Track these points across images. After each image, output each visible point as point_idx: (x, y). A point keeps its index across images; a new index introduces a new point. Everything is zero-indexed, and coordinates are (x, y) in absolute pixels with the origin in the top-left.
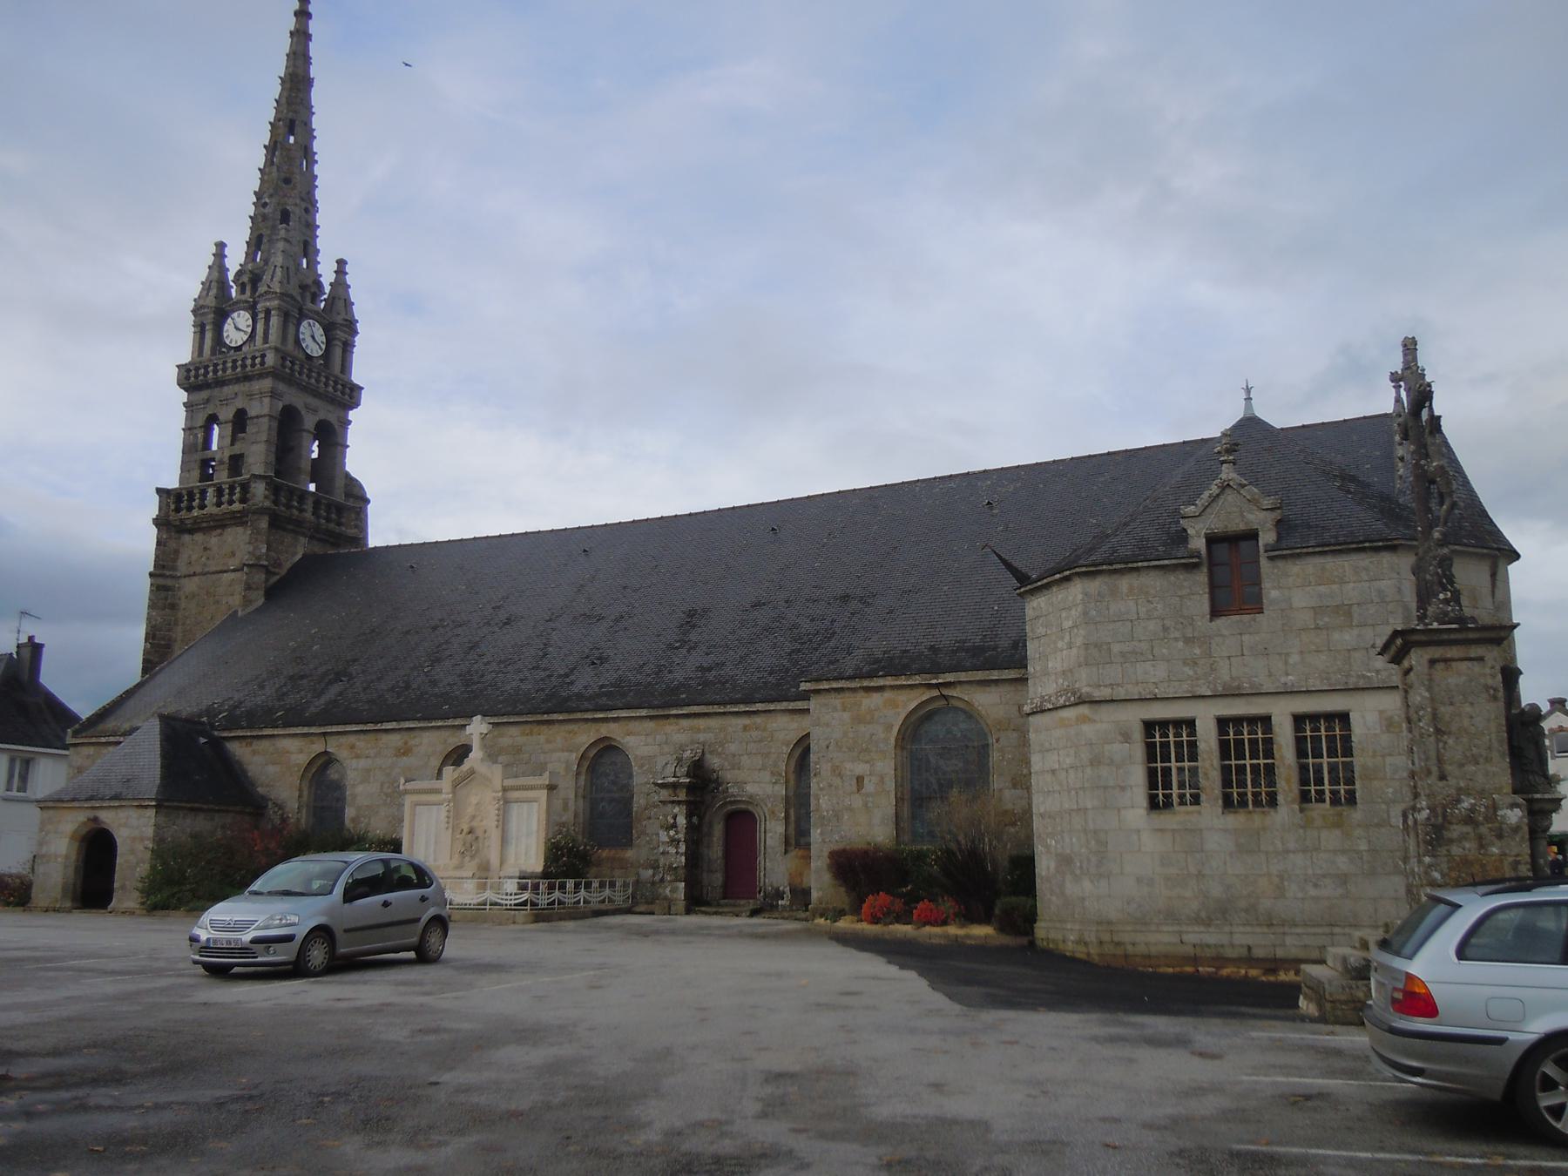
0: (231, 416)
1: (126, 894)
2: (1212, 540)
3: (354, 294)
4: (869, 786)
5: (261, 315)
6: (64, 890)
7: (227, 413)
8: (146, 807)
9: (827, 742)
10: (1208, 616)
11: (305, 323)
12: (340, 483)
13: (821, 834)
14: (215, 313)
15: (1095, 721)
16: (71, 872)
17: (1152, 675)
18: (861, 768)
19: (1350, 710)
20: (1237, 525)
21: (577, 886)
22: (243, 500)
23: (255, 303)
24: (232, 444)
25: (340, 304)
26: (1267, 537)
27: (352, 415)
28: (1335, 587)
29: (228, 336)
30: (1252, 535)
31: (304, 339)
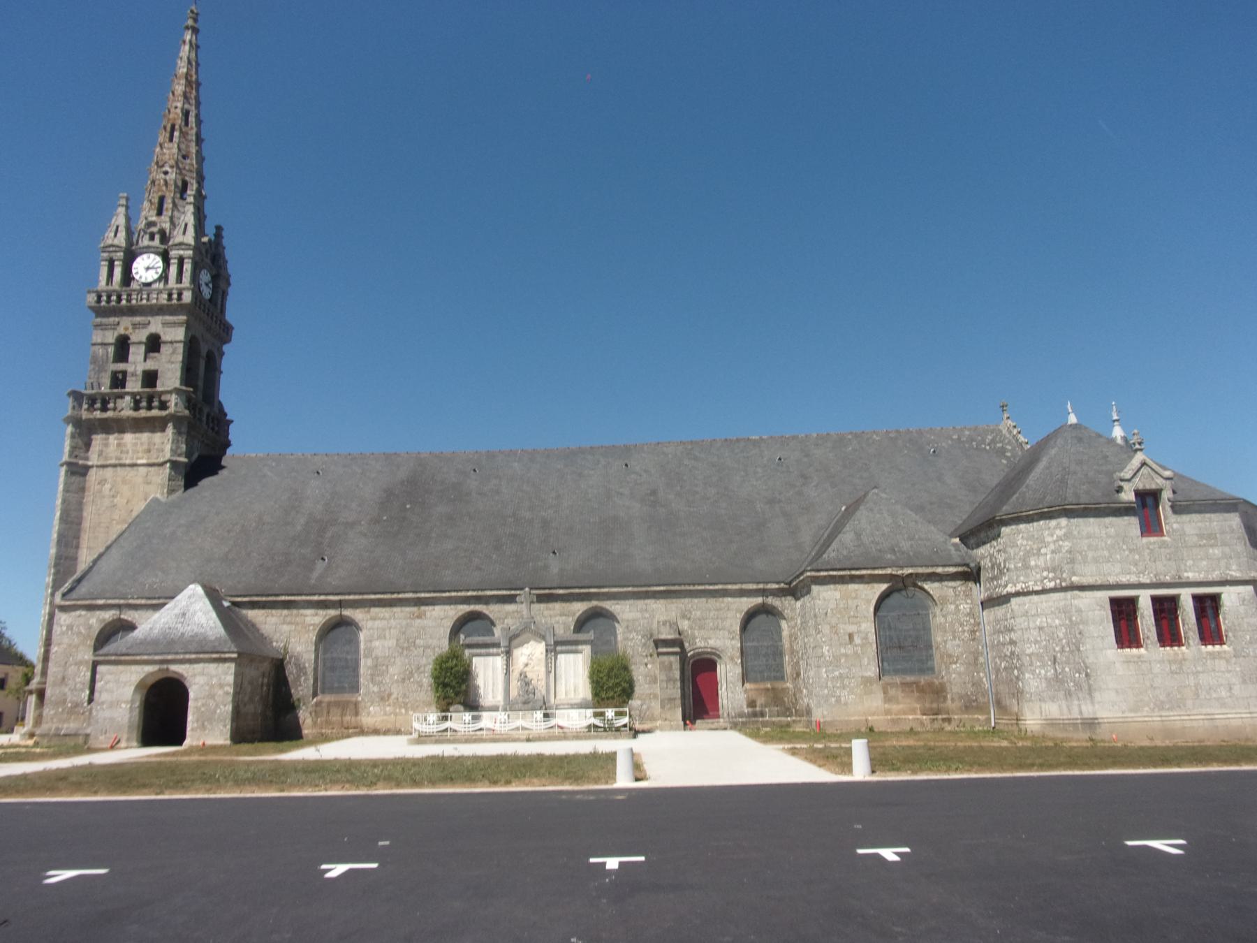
2: (1139, 494)
4: (857, 640)
7: (140, 336)
8: (225, 660)
9: (825, 611)
12: (216, 404)
13: (826, 672)
15: (1082, 598)
16: (136, 713)
20: (1151, 486)
27: (226, 348)
28: (1208, 524)
29: (137, 273)
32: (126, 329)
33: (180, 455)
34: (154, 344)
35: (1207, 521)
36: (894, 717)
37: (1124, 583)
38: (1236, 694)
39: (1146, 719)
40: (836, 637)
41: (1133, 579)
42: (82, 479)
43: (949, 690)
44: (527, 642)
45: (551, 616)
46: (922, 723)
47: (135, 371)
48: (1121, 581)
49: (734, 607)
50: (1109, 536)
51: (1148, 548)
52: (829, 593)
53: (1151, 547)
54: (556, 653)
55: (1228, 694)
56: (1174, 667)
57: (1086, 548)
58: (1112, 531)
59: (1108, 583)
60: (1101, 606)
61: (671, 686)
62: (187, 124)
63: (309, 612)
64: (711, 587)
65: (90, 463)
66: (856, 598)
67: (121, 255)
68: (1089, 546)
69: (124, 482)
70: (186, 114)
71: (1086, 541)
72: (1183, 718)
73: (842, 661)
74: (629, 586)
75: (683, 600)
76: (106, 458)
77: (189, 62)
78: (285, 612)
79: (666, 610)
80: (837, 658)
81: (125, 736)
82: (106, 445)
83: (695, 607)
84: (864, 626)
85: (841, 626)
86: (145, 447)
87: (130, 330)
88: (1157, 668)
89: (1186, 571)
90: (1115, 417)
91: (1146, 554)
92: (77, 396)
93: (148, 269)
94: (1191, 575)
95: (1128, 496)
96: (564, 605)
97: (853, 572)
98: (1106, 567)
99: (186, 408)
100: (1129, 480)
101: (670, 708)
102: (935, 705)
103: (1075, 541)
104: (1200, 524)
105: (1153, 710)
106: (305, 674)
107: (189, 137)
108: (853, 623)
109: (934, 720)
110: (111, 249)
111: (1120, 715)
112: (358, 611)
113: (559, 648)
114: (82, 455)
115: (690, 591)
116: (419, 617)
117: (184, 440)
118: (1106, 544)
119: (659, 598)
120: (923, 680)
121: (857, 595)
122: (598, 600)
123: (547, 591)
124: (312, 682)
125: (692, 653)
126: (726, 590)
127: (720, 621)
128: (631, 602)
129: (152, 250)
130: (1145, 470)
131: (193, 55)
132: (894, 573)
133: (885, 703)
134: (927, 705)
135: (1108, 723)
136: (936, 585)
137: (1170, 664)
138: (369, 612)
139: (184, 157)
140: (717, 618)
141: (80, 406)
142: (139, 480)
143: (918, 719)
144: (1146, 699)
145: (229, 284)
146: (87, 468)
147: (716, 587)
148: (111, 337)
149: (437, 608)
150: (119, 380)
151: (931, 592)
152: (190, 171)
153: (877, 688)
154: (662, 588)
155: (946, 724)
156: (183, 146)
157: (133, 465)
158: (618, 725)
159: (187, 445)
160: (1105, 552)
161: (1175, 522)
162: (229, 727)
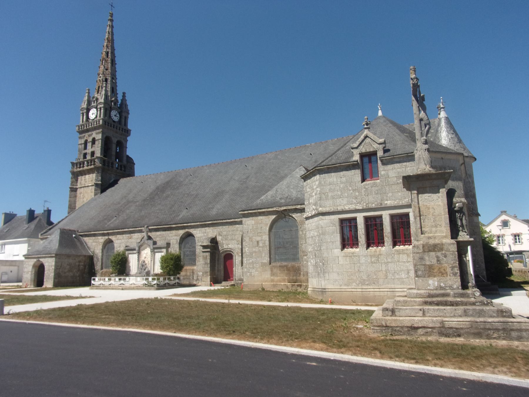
0: (91, 140)
1: (48, 282)
2: (362, 156)
3: (128, 103)
4: (261, 245)
5: (99, 109)
6: (31, 280)
7: (90, 139)
10: (361, 182)
11: (112, 111)
13: (246, 260)
14: (86, 110)
16: (33, 275)
17: (344, 204)
18: (258, 238)
19: (409, 212)
21: (174, 279)
22: (94, 164)
23: (97, 106)
24: (92, 148)
25: (124, 106)
26: (380, 154)
28: (404, 169)
30: (374, 153)
31: (112, 116)
32: (87, 137)
33: (98, 181)
34: (94, 141)
35: (403, 168)
36: (274, 283)
37: (346, 210)
38: (411, 276)
39: (353, 290)
40: (251, 243)
41: (352, 207)
42: (75, 193)
43: (302, 270)
44: (146, 248)
45: (172, 236)
46: (287, 287)
47: (89, 152)
48: (345, 209)
49: (239, 229)
50: (342, 183)
51: (365, 188)
52: (250, 221)
53: (366, 187)
54: (155, 253)
55: (406, 276)
56: (373, 259)
57: (328, 191)
58: (344, 179)
59: (337, 210)
60: (333, 224)
61: (206, 266)
62: (107, 57)
63: (100, 237)
64: (229, 221)
65: (77, 187)
66: (261, 223)
67: (85, 111)
68: (330, 190)
69: (86, 193)
70: (107, 53)
71: (329, 187)
72: (375, 290)
73: (254, 255)
74: (198, 222)
75: (219, 227)
76: (82, 185)
77: (109, 33)
78: (94, 238)
79: (213, 232)
80: (251, 254)
81: (29, 283)
82: (82, 180)
83: (224, 230)
84: (264, 237)
85: (254, 238)
86: (91, 179)
87: (88, 138)
88: (363, 260)
89: (387, 200)
90: (442, 106)
91: (363, 191)
92: (73, 164)
93: (93, 114)
94: (389, 203)
95: (356, 158)
96: (176, 231)
97: (259, 211)
98: (338, 201)
99: (100, 163)
100: (357, 148)
101: (206, 276)
102: (295, 278)
103: (322, 187)
104: (399, 170)
105: (358, 285)
106: (99, 261)
107: (108, 62)
108: (259, 236)
109: (293, 285)
110: (83, 109)
111: (339, 287)
112: (113, 236)
113: (155, 250)
114: (75, 184)
115: (222, 223)
116: (130, 238)
117: (100, 175)
118: (340, 187)
119: (210, 227)
120: (290, 264)
121: (262, 221)
122: (188, 229)
123: (169, 226)
124: (100, 264)
125: (222, 251)
126: (236, 221)
127: (233, 236)
128: (200, 229)
129: (94, 107)
130: (368, 140)
131: (110, 30)
132: (277, 210)
133: (271, 276)
134: (291, 278)
135: (330, 291)
136: (299, 214)
137: (371, 257)
138: (116, 237)
139: (107, 70)
140: (232, 235)
141: (74, 167)
142: (89, 191)
143: (285, 284)
144: (355, 278)
145: (128, 113)
146: (77, 189)
147: (231, 220)
148: (83, 141)
149: (136, 234)
150: (85, 155)
151: (296, 219)
152: (108, 74)
153: (268, 268)
154: (210, 222)
155: (299, 288)
156: (106, 66)
157: (88, 186)
158: (152, 284)
159: (101, 177)
160: (339, 192)
161: (383, 171)
162: (53, 281)
